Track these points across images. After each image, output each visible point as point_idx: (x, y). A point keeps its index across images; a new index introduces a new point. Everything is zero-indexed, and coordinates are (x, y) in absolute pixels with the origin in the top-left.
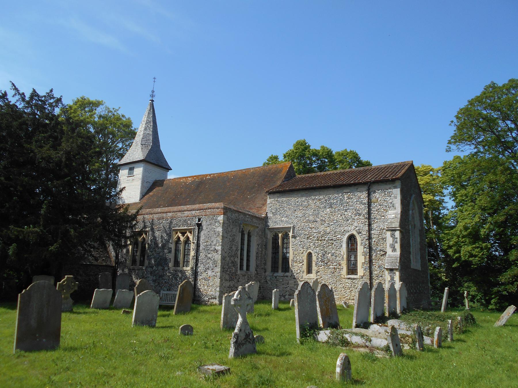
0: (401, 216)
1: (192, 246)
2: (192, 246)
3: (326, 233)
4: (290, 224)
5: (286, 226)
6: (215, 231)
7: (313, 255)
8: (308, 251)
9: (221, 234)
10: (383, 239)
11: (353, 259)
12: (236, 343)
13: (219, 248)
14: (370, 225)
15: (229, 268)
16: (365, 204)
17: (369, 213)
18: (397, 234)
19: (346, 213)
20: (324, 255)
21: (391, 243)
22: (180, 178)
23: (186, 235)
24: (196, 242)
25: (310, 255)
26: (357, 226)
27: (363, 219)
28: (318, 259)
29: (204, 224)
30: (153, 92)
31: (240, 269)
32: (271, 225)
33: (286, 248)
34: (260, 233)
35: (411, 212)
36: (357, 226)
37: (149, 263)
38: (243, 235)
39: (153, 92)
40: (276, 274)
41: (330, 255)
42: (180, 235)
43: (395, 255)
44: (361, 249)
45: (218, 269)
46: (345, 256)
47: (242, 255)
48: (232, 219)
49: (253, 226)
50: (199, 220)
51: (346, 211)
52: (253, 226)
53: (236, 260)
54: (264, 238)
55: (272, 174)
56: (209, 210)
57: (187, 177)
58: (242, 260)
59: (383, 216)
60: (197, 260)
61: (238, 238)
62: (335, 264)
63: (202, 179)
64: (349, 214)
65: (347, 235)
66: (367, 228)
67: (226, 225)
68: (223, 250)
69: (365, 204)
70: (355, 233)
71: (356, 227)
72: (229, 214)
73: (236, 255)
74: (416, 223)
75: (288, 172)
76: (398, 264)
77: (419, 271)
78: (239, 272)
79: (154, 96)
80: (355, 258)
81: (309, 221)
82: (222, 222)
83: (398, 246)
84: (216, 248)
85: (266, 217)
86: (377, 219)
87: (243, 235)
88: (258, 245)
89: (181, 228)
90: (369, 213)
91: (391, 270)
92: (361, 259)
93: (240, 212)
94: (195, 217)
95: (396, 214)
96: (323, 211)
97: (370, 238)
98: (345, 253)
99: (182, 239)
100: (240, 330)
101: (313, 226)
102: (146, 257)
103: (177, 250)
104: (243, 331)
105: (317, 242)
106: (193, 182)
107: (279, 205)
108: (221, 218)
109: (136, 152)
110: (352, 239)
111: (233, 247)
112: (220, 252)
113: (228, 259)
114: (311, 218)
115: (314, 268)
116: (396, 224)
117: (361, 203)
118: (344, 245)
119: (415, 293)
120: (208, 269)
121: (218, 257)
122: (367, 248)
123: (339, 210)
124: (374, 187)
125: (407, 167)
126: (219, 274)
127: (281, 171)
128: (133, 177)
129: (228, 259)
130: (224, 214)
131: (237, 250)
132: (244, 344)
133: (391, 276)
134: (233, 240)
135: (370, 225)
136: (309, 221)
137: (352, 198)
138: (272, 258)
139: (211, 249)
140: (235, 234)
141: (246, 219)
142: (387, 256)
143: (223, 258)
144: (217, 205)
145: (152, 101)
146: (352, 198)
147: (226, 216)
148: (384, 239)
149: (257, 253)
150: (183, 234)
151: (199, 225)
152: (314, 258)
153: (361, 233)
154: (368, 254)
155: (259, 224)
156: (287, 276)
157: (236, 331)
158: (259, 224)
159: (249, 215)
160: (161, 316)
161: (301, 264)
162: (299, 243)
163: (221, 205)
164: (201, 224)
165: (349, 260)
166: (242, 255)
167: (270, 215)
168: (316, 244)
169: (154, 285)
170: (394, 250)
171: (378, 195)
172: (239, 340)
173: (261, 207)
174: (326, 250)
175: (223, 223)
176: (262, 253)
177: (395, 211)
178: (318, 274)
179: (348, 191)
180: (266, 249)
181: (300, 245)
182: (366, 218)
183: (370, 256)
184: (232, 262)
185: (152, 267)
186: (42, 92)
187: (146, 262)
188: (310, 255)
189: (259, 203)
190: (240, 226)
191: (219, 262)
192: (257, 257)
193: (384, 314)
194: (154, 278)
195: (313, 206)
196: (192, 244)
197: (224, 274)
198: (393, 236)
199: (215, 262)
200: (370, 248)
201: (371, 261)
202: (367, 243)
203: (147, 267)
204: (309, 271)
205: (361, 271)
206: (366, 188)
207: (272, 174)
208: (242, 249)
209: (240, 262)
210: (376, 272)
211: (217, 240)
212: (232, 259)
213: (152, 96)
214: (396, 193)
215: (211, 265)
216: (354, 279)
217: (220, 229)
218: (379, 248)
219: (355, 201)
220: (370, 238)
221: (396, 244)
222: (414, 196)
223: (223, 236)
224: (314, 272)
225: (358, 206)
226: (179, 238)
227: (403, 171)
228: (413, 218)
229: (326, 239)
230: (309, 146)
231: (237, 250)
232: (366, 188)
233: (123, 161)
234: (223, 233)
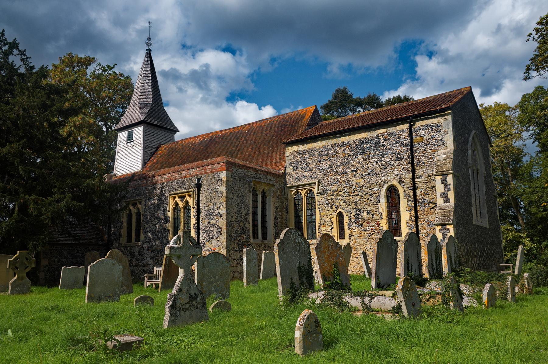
0: (454, 155)
1: (193, 212)
2: (193, 212)
4: (314, 178)
6: (217, 192)
7: (345, 215)
8: (338, 211)
9: (224, 194)
10: (432, 188)
11: (394, 216)
12: (172, 307)
13: (223, 211)
14: (413, 172)
15: (238, 236)
16: (406, 145)
17: (412, 157)
18: (450, 179)
19: (383, 159)
20: (358, 214)
21: (443, 191)
23: (185, 200)
24: (196, 207)
25: (340, 215)
26: (396, 175)
28: (350, 220)
29: (204, 183)
31: (254, 238)
32: (290, 181)
33: (312, 209)
34: (279, 193)
35: (470, 152)
37: (145, 237)
38: (255, 195)
39: (149, 39)
42: (178, 200)
43: (448, 206)
44: (404, 204)
45: (223, 238)
46: (385, 214)
47: (255, 220)
48: (238, 175)
49: (268, 184)
50: (199, 180)
51: (383, 156)
52: (268, 184)
53: (247, 225)
54: (284, 199)
55: (293, 122)
56: (210, 167)
57: (195, 137)
58: (255, 226)
59: (431, 158)
61: (249, 199)
62: (372, 224)
63: (211, 137)
64: (386, 159)
65: (386, 186)
66: (410, 176)
67: (230, 183)
68: (228, 213)
69: (406, 145)
70: (395, 183)
71: (397, 175)
72: (234, 170)
73: (246, 220)
74: (479, 167)
75: (311, 118)
76: (452, 217)
77: (485, 228)
78: (252, 241)
79: (151, 44)
80: (397, 215)
81: (337, 173)
82: (224, 179)
83: (451, 195)
84: (221, 212)
85: (285, 174)
86: (423, 163)
87: (255, 195)
88: (276, 208)
89: (179, 192)
90: (412, 157)
91: (443, 225)
93: (250, 167)
94: (194, 176)
95: (448, 153)
96: (354, 160)
97: (414, 188)
98: (384, 210)
99: (181, 204)
100: (180, 290)
101: (343, 179)
102: (141, 231)
103: (176, 219)
104: (184, 291)
105: (348, 198)
106: (201, 143)
107: (300, 158)
108: (223, 175)
109: (133, 113)
110: (392, 192)
111: (242, 210)
112: (224, 217)
113: (236, 225)
114: (340, 169)
115: (347, 232)
116: (448, 166)
117: (402, 144)
118: (383, 200)
119: (481, 256)
120: (212, 238)
121: (222, 223)
122: (412, 201)
123: (374, 156)
125: (462, 95)
126: (224, 243)
127: (303, 117)
128: (133, 143)
129: (236, 225)
130: (227, 170)
131: (247, 214)
132: (187, 309)
133: (443, 234)
134: (242, 202)
135: (413, 172)
136: (337, 173)
137: (389, 140)
138: (295, 223)
139: (214, 214)
140: (243, 194)
141: (258, 176)
142: (438, 209)
143: (229, 224)
144: (219, 159)
145: (149, 50)
146: (389, 140)
147: (230, 172)
148: (433, 188)
149: (275, 218)
150: (182, 198)
151: (199, 186)
152: (346, 219)
153: (403, 182)
154: (413, 209)
155: (276, 182)
157: (174, 291)
158: (276, 182)
159: (262, 171)
161: (330, 228)
162: (327, 202)
163: (222, 159)
164: (201, 184)
165: (390, 217)
166: (255, 220)
167: (289, 170)
168: (348, 202)
169: (152, 263)
170: (447, 200)
172: (178, 303)
173: (279, 162)
174: (360, 208)
175: (227, 181)
176: (282, 218)
177: (446, 151)
178: (352, 238)
180: (287, 212)
181: (328, 204)
182: (409, 163)
183: (416, 212)
184: (242, 229)
185: (149, 242)
187: (142, 237)
188: (340, 215)
189: (276, 157)
190: (249, 185)
191: (224, 231)
192: (275, 222)
193: (421, 275)
194: (152, 254)
195: (341, 153)
196: (192, 209)
197: (232, 243)
198: (444, 182)
199: (219, 229)
200: (415, 200)
201: (417, 217)
202: (412, 194)
203: (143, 242)
207: (293, 122)
208: (255, 214)
209: (254, 229)
210: (425, 231)
211: (221, 203)
212: (241, 224)
213: (149, 44)
214: (446, 122)
215: (215, 233)
217: (223, 188)
218: (428, 200)
219: (394, 142)
220: (414, 188)
221: (449, 192)
222: (474, 132)
223: (227, 197)
224: (347, 236)
225: (399, 149)
226: (176, 204)
227: (457, 99)
228: (475, 161)
229: (360, 194)
230: (351, 95)
231: (247, 214)
233: (119, 126)
234: (227, 193)
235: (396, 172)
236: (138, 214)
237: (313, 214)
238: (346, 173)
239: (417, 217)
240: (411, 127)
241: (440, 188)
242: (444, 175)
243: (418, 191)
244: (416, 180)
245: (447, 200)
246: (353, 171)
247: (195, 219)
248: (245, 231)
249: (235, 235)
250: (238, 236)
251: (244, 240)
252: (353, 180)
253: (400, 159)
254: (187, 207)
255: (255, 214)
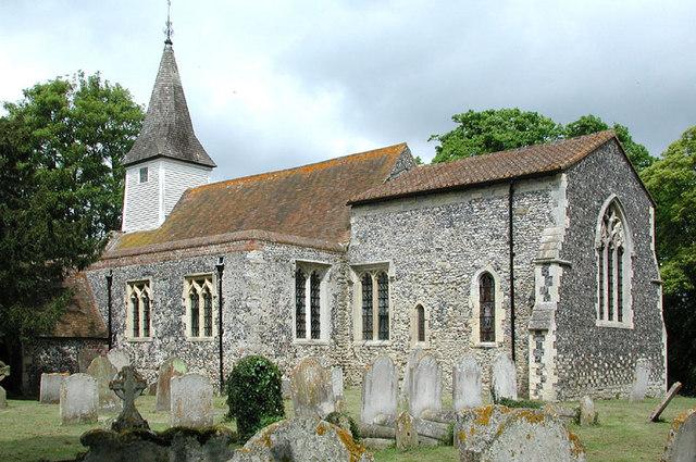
1: (215, 303)
2: (215, 303)
3: (445, 272)
5: (380, 261)
11: (487, 314)
14: (512, 255)
22: (225, 183)
25: (420, 308)
26: (491, 258)
27: (502, 244)
30: (169, 24)
36: (491, 258)
39: (169, 24)
40: (369, 343)
41: (451, 308)
44: (500, 298)
50: (221, 259)
57: (237, 180)
60: (221, 323)
65: (478, 272)
71: (493, 259)
78: (296, 341)
92: (501, 314)
99: (199, 290)
101: (424, 260)
106: (246, 189)
110: (487, 280)
114: (421, 245)
120: (239, 338)
124: (522, 189)
145: (168, 42)
150: (201, 283)
151: (220, 269)
152: (427, 315)
156: (385, 346)
160: (620, 320)
165: (482, 317)
166: (300, 314)
170: (547, 297)
171: (527, 203)
179: (479, 195)
184: (280, 326)
186: (587, 116)
188: (420, 308)
198: (545, 273)
200: (512, 295)
201: (513, 318)
204: (422, 338)
205: (500, 334)
206: (505, 192)
213: (169, 33)
216: (489, 348)
224: (427, 338)
230: (418, 160)
232: (505, 192)
235: (491, 255)
236: (146, 301)
237: (386, 307)
238: (429, 251)
239: (513, 318)
240: (512, 192)
241: (540, 281)
242: (546, 264)
243: (517, 283)
244: (515, 267)
245: (547, 297)
246: (438, 249)
247: (218, 311)
248: (284, 329)
249: (270, 334)
250: (275, 335)
251: (284, 341)
252: (438, 263)
253: (498, 237)
254: (208, 297)
255: (300, 306)
